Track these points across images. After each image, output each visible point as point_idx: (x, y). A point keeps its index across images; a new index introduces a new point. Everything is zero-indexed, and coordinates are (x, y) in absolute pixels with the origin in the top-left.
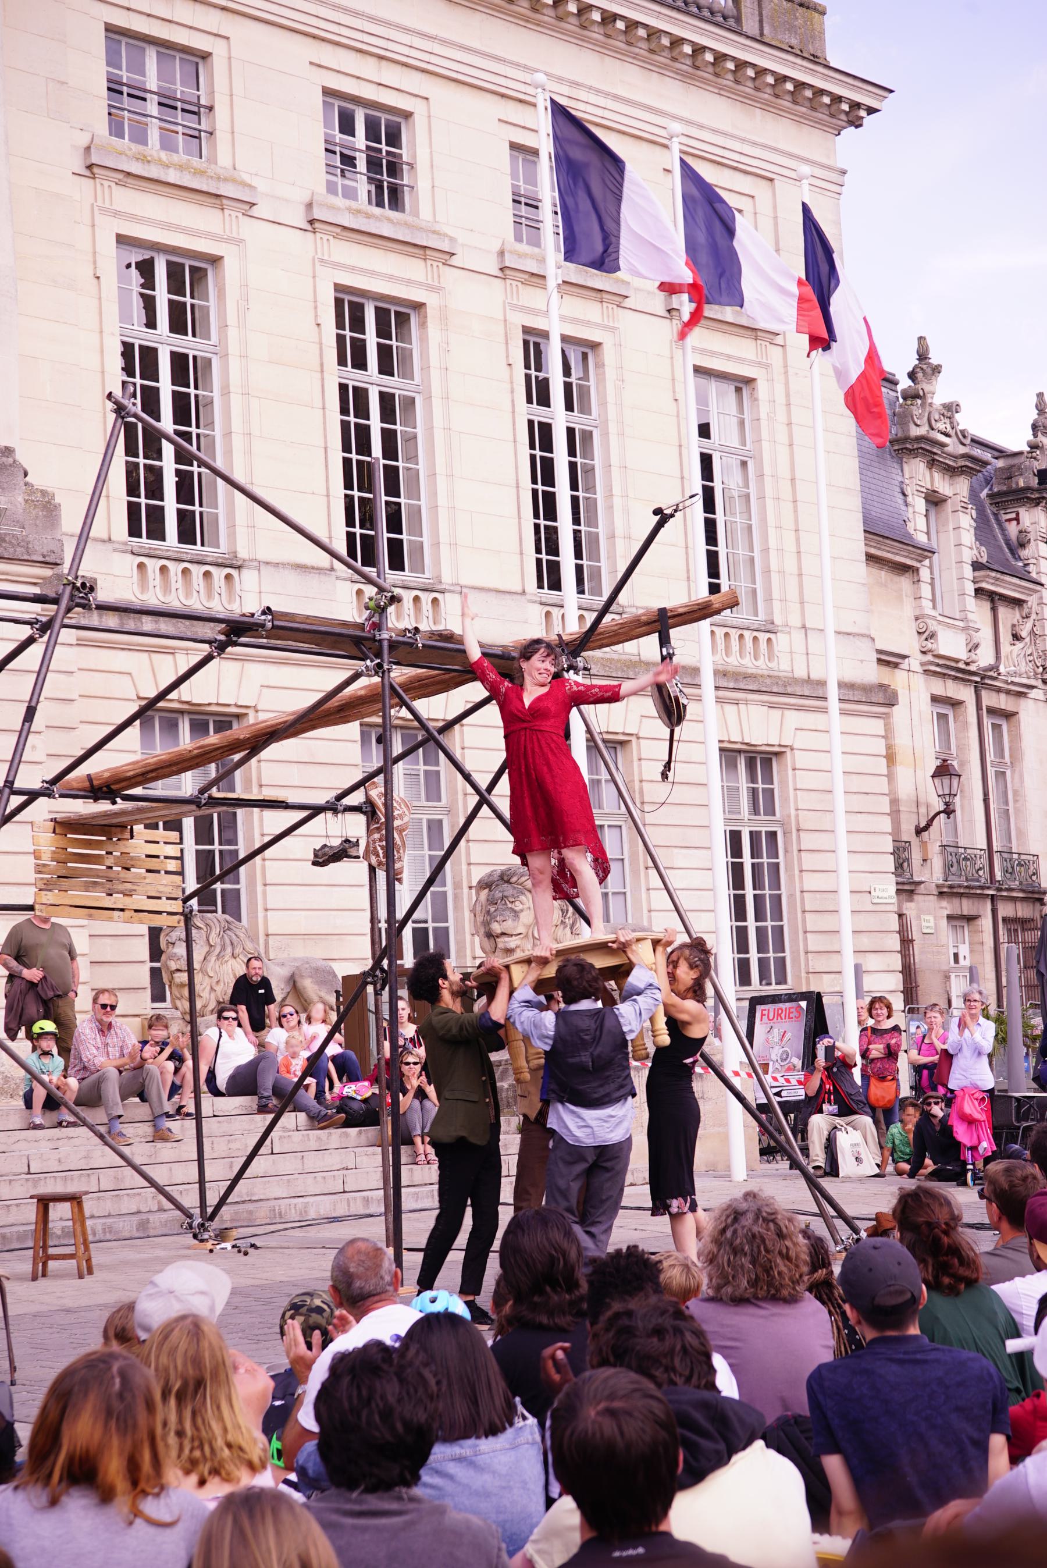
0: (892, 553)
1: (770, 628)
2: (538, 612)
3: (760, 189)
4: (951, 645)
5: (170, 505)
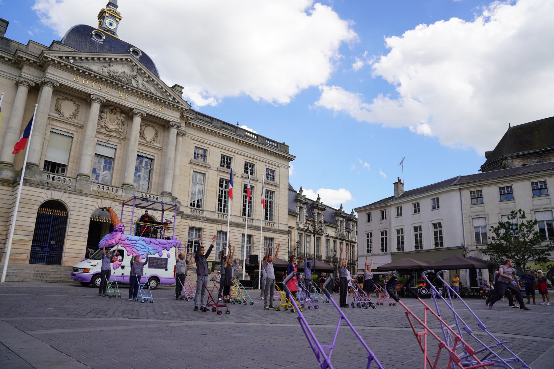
0: (292, 214)
1: (274, 223)
2: (242, 219)
3: (278, 168)
4: (301, 226)
5: (223, 208)
